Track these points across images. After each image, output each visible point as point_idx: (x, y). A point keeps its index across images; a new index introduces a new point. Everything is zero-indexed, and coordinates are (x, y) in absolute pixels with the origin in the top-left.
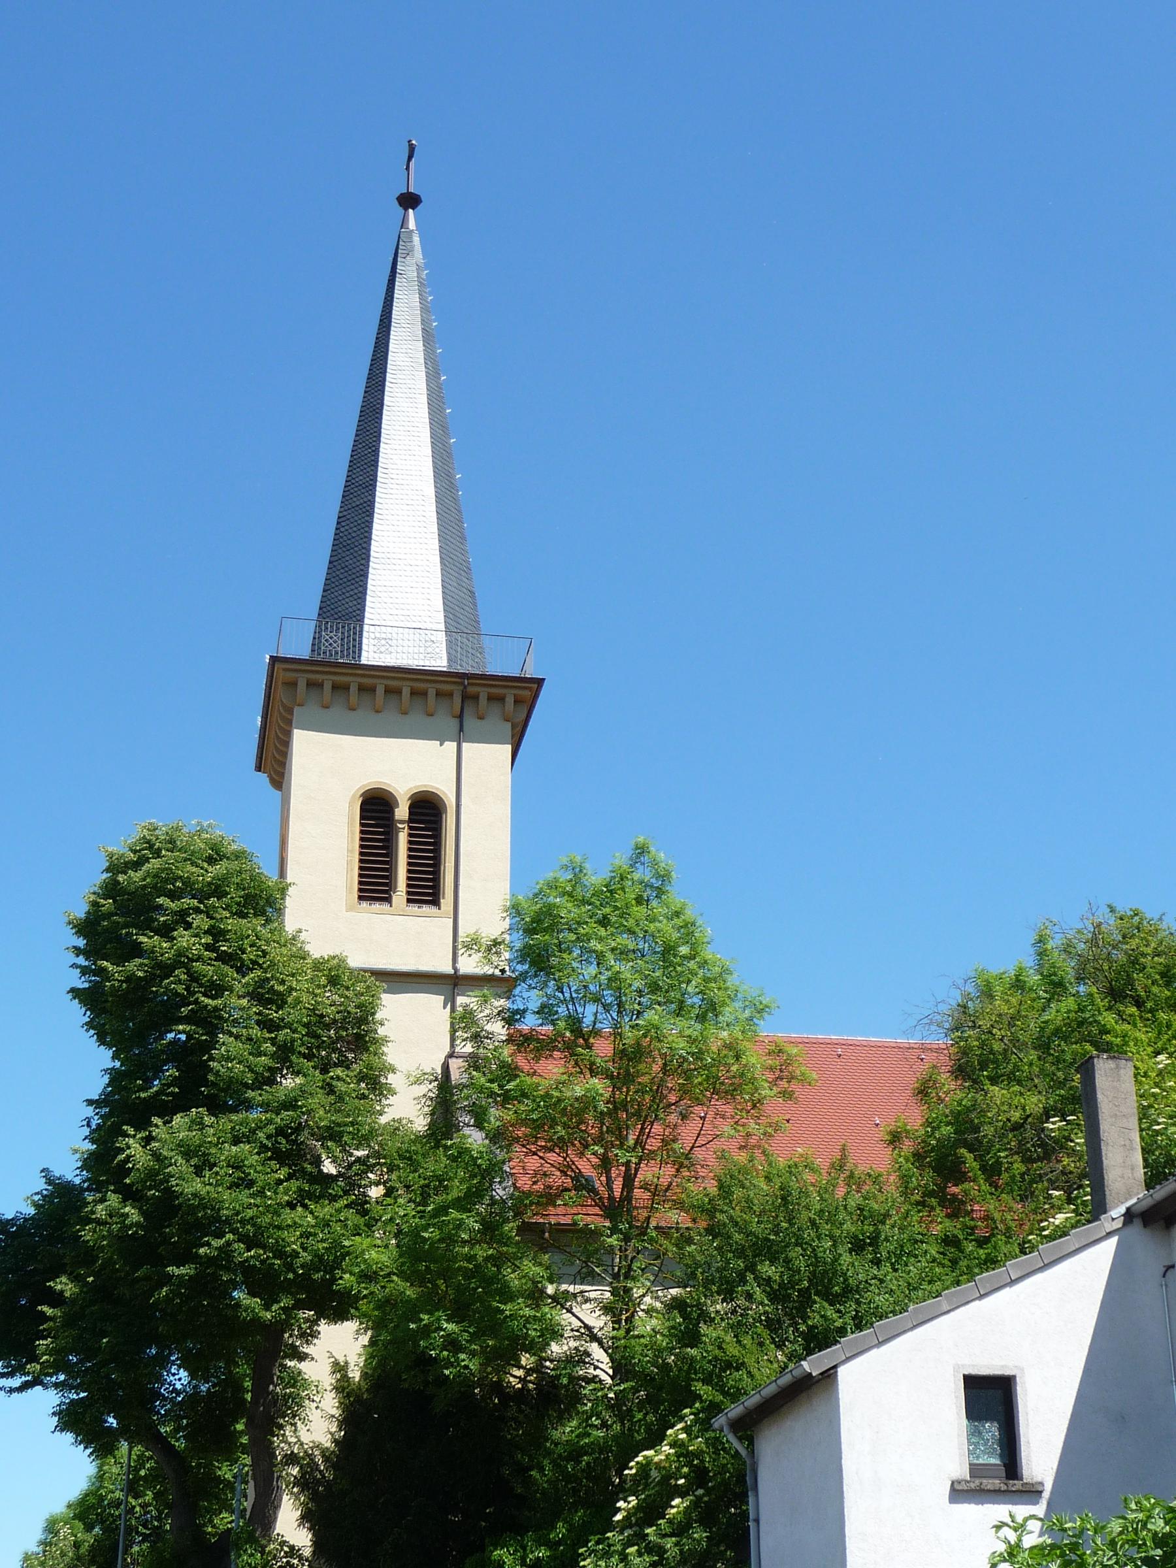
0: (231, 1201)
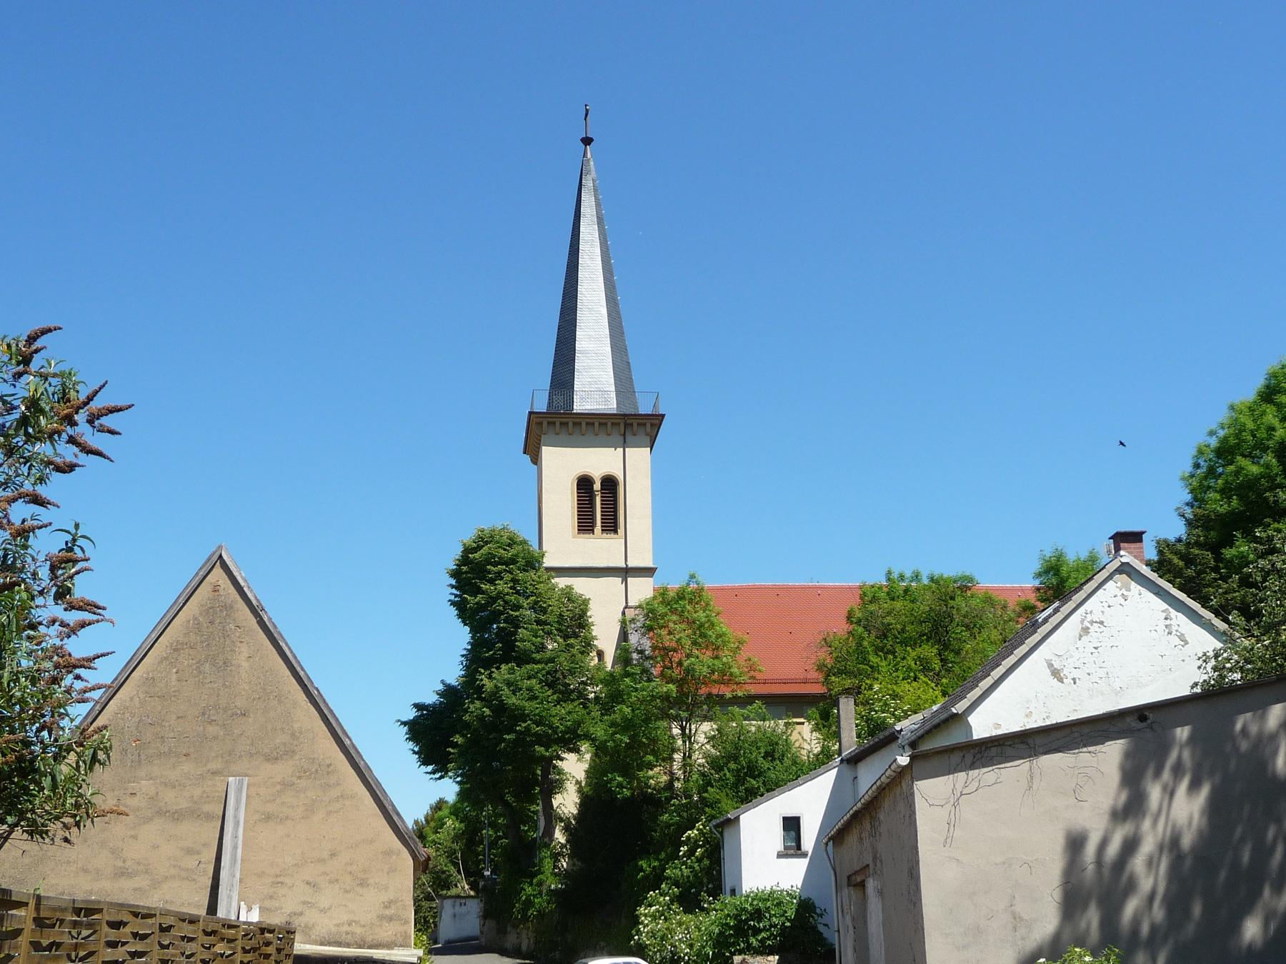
0: (529, 706)
